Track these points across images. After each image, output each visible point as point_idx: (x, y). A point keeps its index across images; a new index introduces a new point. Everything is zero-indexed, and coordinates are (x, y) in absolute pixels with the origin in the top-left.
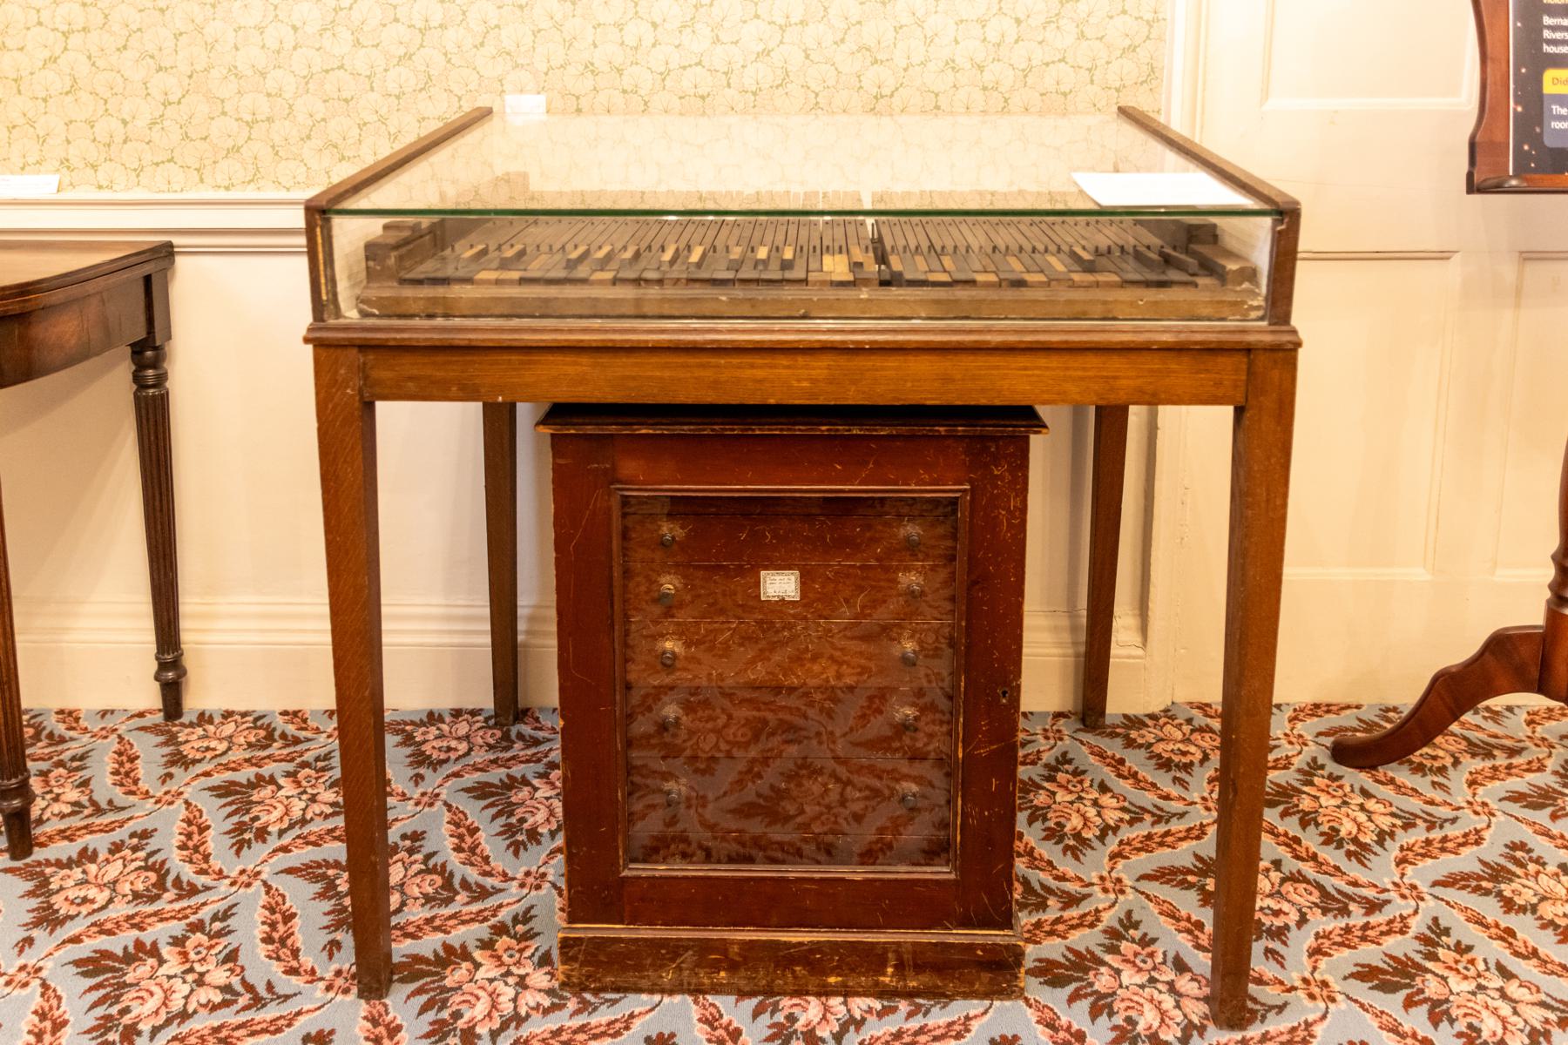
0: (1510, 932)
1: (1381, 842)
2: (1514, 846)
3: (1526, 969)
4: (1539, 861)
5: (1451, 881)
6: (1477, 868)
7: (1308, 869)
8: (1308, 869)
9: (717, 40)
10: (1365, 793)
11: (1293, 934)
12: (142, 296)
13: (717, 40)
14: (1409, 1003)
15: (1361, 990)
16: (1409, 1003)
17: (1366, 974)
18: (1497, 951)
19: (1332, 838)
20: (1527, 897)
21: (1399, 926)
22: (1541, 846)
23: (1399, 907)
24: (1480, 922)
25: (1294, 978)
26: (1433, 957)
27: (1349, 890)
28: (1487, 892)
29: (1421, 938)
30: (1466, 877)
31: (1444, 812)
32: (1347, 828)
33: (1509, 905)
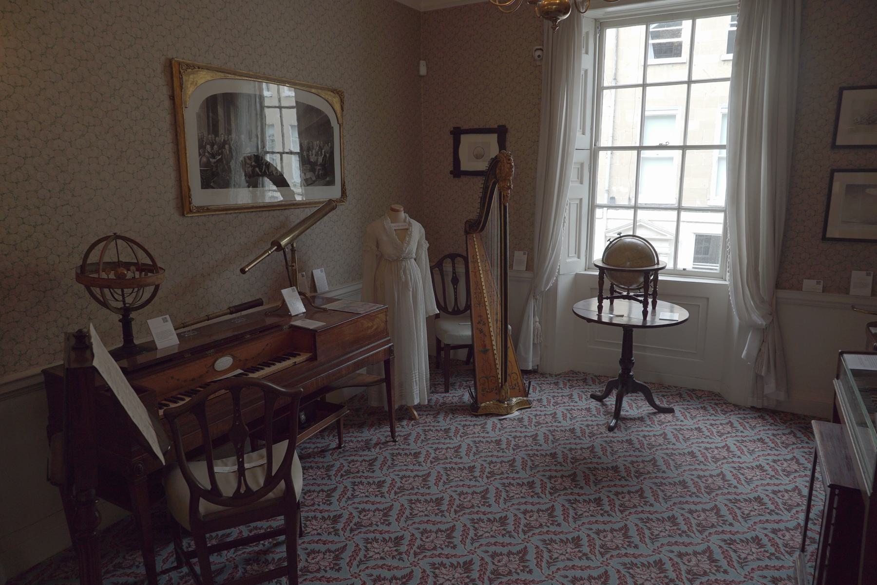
0: (324, 544)
1: (366, 547)
2: (331, 503)
3: (316, 538)
4: (324, 503)
5: (335, 489)
6: (342, 556)
7: (313, 508)
8: (313, 508)
9: (73, 196)
10: (319, 534)
11: (306, 556)
12: (695, 151)
13: (9, 233)
14: (329, 516)
15: (339, 513)
16: (273, 559)
17: (340, 516)
18: (324, 538)
19: (315, 518)
20: (321, 494)
21: (389, 492)
22: (326, 507)
23: (338, 478)
24: (325, 485)
25: (350, 507)
26: (333, 528)
27: (305, 577)
28: (336, 551)
29: (338, 530)
30: (342, 552)
31: (363, 567)
32: (314, 522)
33: (329, 551)
